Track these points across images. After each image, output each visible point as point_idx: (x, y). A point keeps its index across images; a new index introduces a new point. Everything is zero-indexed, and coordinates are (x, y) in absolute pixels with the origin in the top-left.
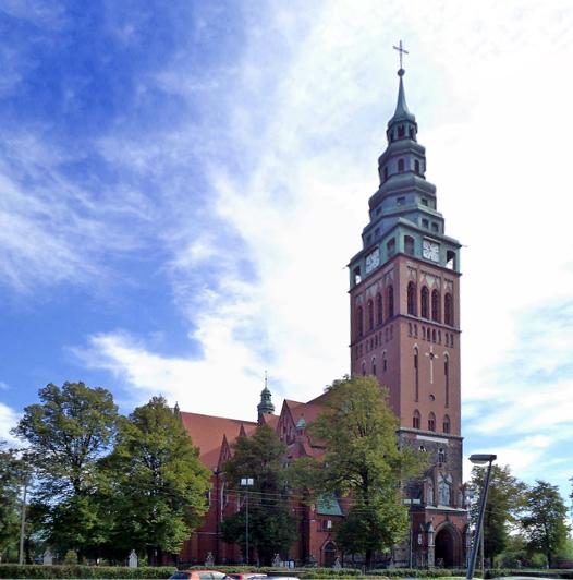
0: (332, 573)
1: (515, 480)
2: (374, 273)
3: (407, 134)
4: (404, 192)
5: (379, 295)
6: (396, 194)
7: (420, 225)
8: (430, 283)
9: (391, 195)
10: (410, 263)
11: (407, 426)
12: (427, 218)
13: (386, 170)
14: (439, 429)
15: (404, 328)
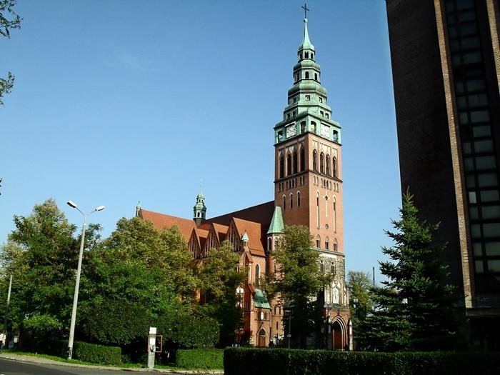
2: (289, 140)
3: (310, 57)
4: (310, 93)
6: (305, 93)
7: (319, 115)
8: (325, 150)
9: (303, 93)
10: (314, 138)
11: (129, 321)
12: (323, 110)
14: (331, 248)
15: (311, 176)
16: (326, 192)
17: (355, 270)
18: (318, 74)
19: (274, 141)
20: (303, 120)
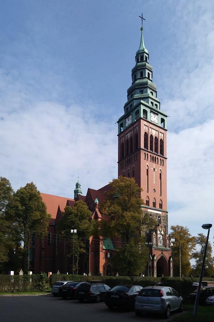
5: (131, 137)
7: (150, 105)
10: (146, 123)
12: (153, 101)
13: (135, 76)
16: (154, 165)
17: (175, 225)
18: (150, 73)
19: (129, 84)
20: (142, 89)
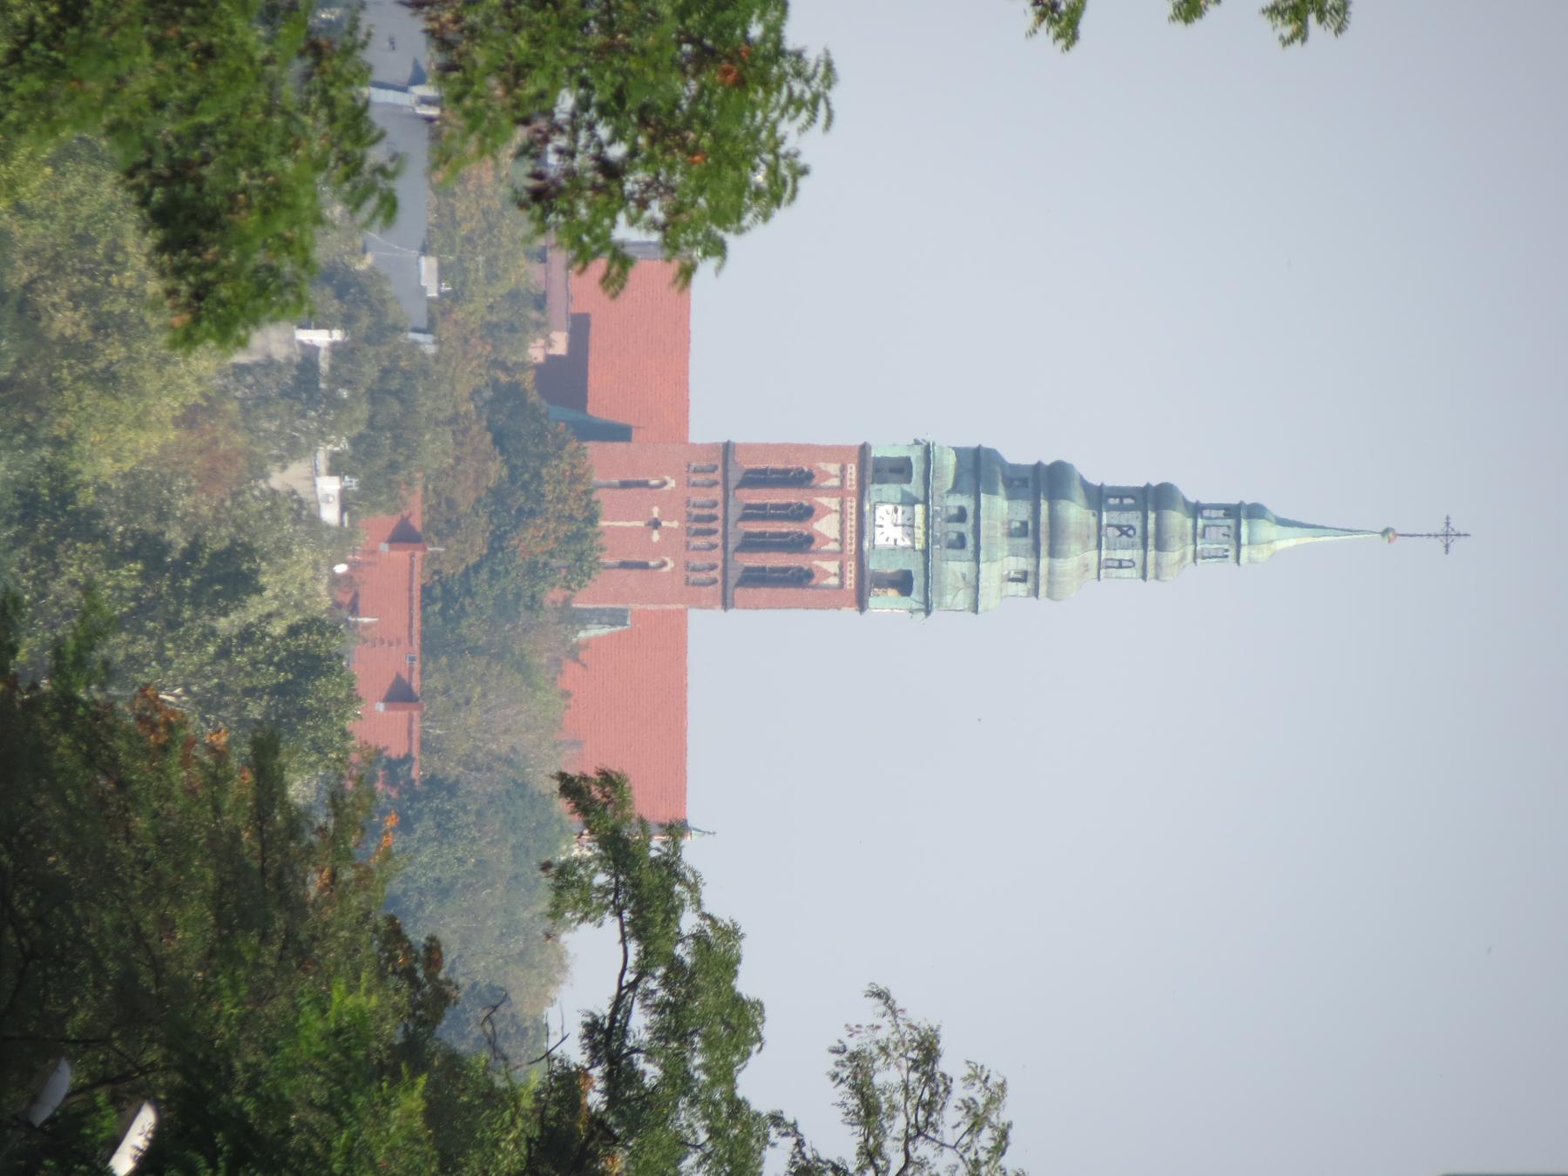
0: (412, 659)
1: (426, 31)
8: (826, 526)
